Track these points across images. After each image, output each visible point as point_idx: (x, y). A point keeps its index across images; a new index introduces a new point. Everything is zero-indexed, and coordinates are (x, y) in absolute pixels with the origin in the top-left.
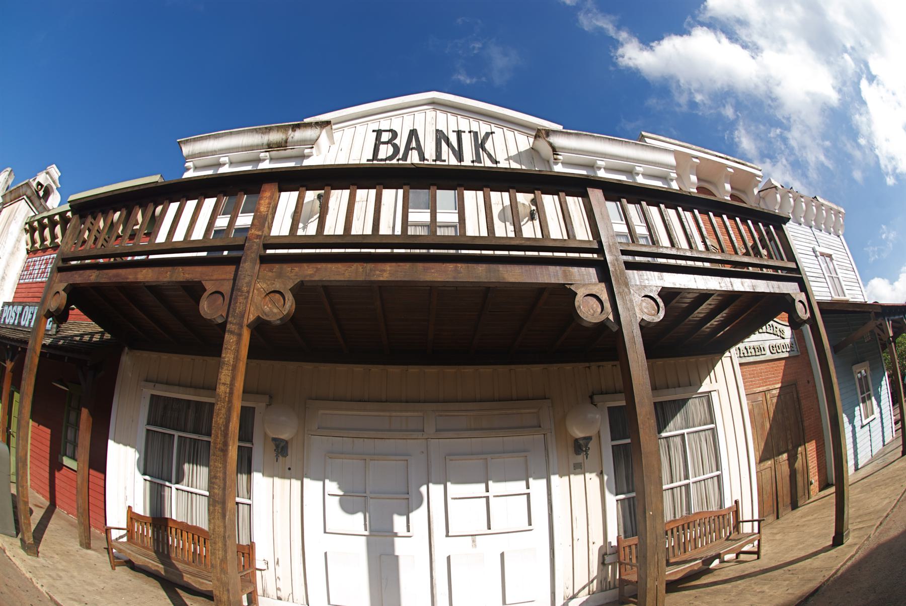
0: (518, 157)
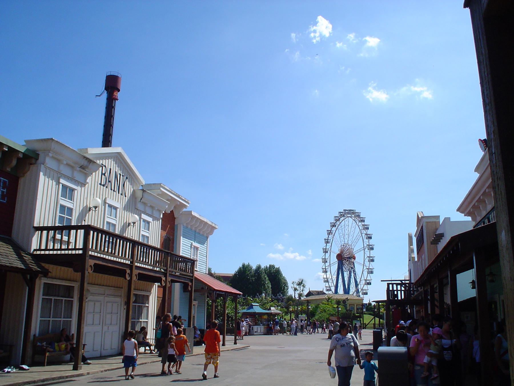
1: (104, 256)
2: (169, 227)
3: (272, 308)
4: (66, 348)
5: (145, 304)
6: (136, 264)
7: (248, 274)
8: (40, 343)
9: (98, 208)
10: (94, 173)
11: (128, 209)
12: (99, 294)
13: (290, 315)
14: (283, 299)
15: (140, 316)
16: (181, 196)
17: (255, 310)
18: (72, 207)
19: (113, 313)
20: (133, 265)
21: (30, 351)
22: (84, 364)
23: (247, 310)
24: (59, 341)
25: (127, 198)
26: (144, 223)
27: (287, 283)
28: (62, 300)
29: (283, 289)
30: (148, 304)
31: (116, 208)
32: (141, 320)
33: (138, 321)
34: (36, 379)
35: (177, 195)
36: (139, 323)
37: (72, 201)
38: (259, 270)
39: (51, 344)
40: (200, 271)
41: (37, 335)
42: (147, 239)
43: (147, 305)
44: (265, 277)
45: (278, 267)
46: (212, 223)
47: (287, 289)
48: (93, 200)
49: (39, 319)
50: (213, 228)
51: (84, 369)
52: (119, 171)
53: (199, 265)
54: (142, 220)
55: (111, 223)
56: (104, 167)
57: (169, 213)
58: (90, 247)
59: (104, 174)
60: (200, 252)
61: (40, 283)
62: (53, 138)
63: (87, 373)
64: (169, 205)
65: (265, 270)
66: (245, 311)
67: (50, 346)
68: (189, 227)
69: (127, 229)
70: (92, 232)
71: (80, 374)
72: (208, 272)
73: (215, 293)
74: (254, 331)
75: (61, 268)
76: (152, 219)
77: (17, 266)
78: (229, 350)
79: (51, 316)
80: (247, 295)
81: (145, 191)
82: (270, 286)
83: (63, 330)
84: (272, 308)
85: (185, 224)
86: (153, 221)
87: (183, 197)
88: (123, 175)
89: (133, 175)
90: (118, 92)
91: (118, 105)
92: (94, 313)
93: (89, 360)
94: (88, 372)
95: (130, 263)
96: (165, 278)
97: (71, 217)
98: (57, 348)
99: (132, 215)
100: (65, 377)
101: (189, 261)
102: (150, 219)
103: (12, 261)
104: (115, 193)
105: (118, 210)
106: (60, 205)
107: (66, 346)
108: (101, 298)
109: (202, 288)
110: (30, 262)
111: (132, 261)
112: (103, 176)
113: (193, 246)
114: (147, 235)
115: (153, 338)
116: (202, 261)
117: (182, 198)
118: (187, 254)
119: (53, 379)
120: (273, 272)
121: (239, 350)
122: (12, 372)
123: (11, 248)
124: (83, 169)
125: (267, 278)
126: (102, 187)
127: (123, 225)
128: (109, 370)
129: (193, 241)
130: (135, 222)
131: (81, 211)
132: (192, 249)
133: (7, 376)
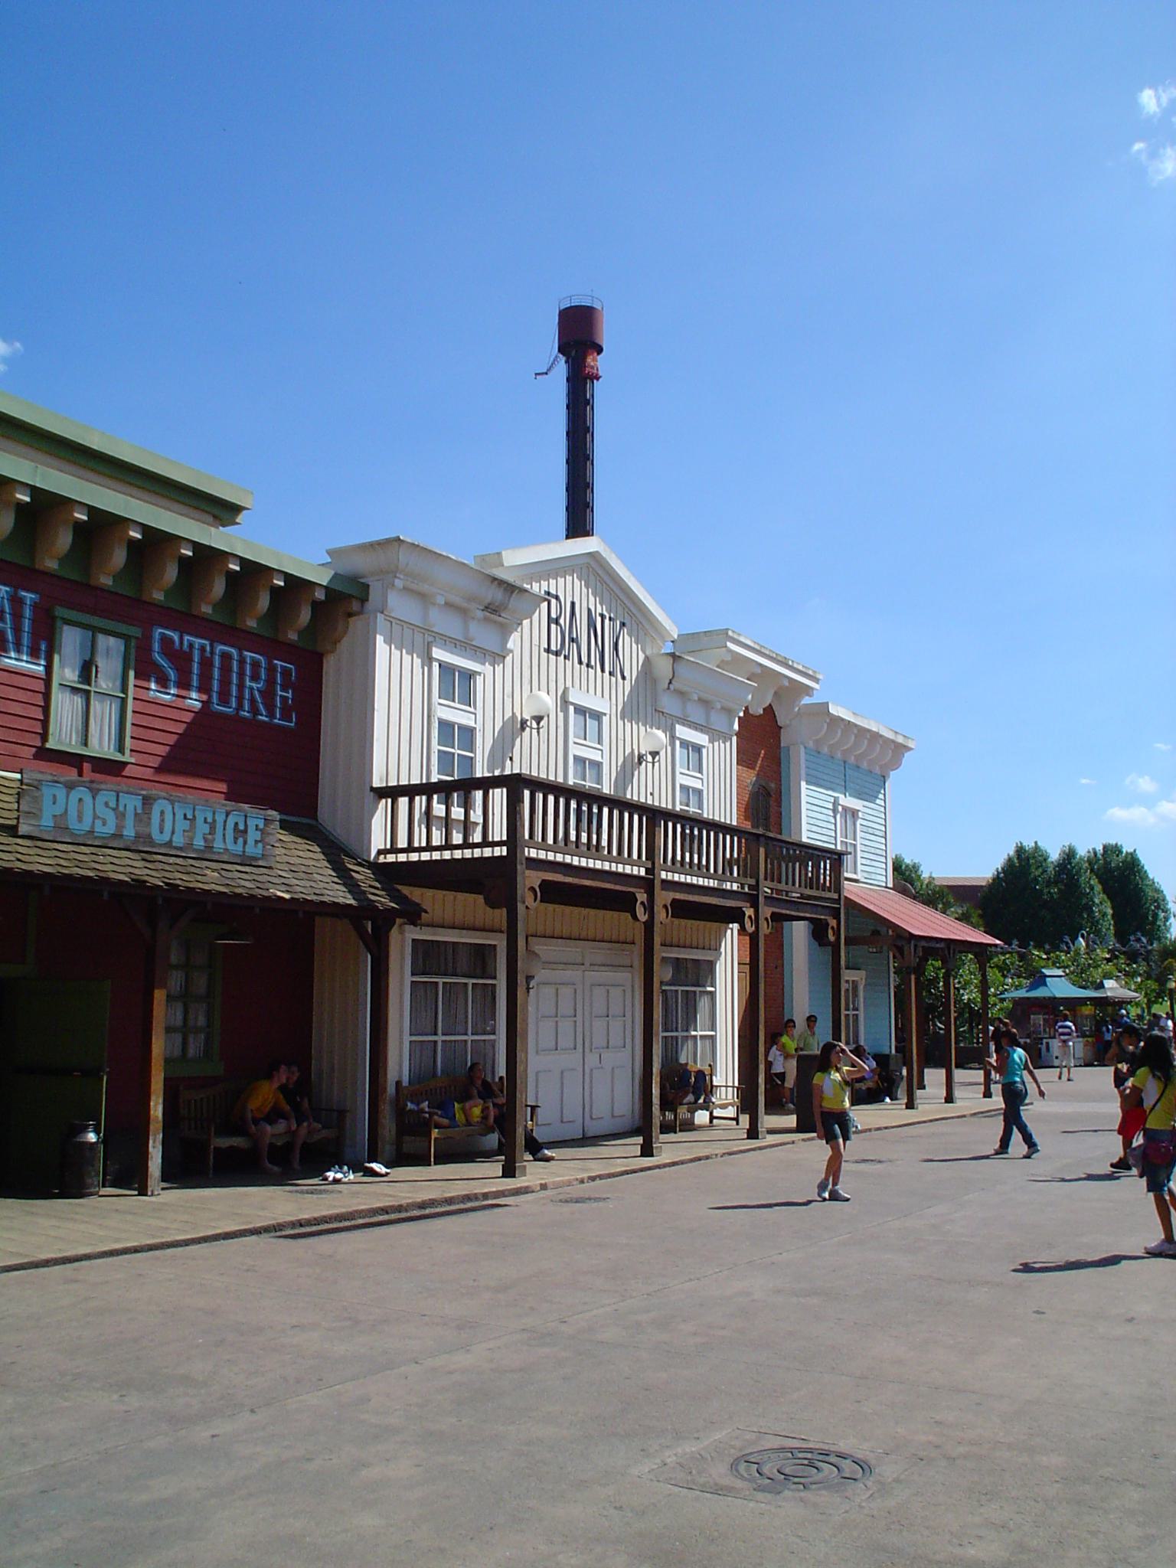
0: (74, 671)
1: (568, 859)
2: (762, 755)
3: (1109, 984)
4: (485, 1117)
5: (704, 986)
6: (663, 875)
7: (1035, 879)
8: (412, 1102)
9: (546, 719)
10: (526, 622)
11: (635, 716)
12: (565, 964)
13: (1169, 1003)
14: (1149, 952)
15: (690, 1021)
16: (793, 662)
17: (1053, 990)
18: (472, 724)
19: (613, 1016)
20: (654, 879)
21: (388, 1127)
22: (535, 1160)
23: (1027, 991)
24: (465, 1097)
25: (627, 682)
26: (686, 751)
27: (1164, 900)
28: (466, 984)
29: (1150, 918)
30: (713, 985)
31: (597, 716)
32: (693, 1033)
33: (687, 1036)
34: (404, 1202)
35: (779, 658)
36: (690, 1043)
37: (470, 706)
38: (1070, 863)
39: (443, 1106)
40: (865, 881)
41: (405, 1082)
42: (696, 798)
43: (709, 989)
44: (1092, 882)
45: (1131, 850)
46: (896, 733)
47: (1166, 919)
48: (529, 697)
49: (407, 1039)
50: (898, 750)
51: (533, 1173)
52: (598, 605)
53: (864, 861)
54: (678, 743)
55: (586, 759)
56: (553, 601)
57: (760, 715)
58: (527, 836)
59: (557, 622)
60: (865, 823)
61: (402, 941)
62: (401, 538)
63: (541, 1184)
64: (754, 691)
65: (1090, 861)
66: (1022, 993)
67: (440, 1112)
68: (825, 750)
69: (636, 773)
70: (527, 793)
71: (521, 1188)
72: (894, 885)
73: (916, 946)
74: (1052, 1056)
75: (455, 897)
76: (707, 737)
77: (336, 900)
78: (964, 1116)
79: (440, 1031)
80: (1032, 943)
81: (679, 657)
82: (1110, 911)
83: (473, 1065)
84: (1109, 984)
85: (811, 744)
86: (710, 742)
87: (798, 664)
88: (612, 615)
89: (640, 610)
90: (598, 354)
91: (601, 393)
92: (557, 1016)
93: (547, 1149)
94: (543, 1182)
95: (646, 873)
96: (752, 910)
97: (472, 752)
98: (459, 1116)
99: (648, 730)
100: (480, 1197)
101: (824, 854)
102: (701, 739)
103: (322, 885)
104: (593, 671)
105: (606, 720)
106: (439, 722)
107: (482, 1111)
108: (569, 974)
109: (876, 933)
110: (371, 886)
111: (650, 866)
112: (553, 626)
113: (840, 808)
114: (698, 785)
115: (734, 1083)
116: (873, 850)
117: (795, 665)
118: (824, 831)
119: (450, 1201)
120: (1118, 867)
121: (995, 1115)
122: (346, 1180)
123: (319, 850)
124: (495, 611)
125: (1098, 888)
126: (552, 657)
127: (624, 761)
128: (601, 1177)
129: (841, 793)
130: (657, 750)
131: (499, 732)
132: (838, 816)
133: (332, 1192)
